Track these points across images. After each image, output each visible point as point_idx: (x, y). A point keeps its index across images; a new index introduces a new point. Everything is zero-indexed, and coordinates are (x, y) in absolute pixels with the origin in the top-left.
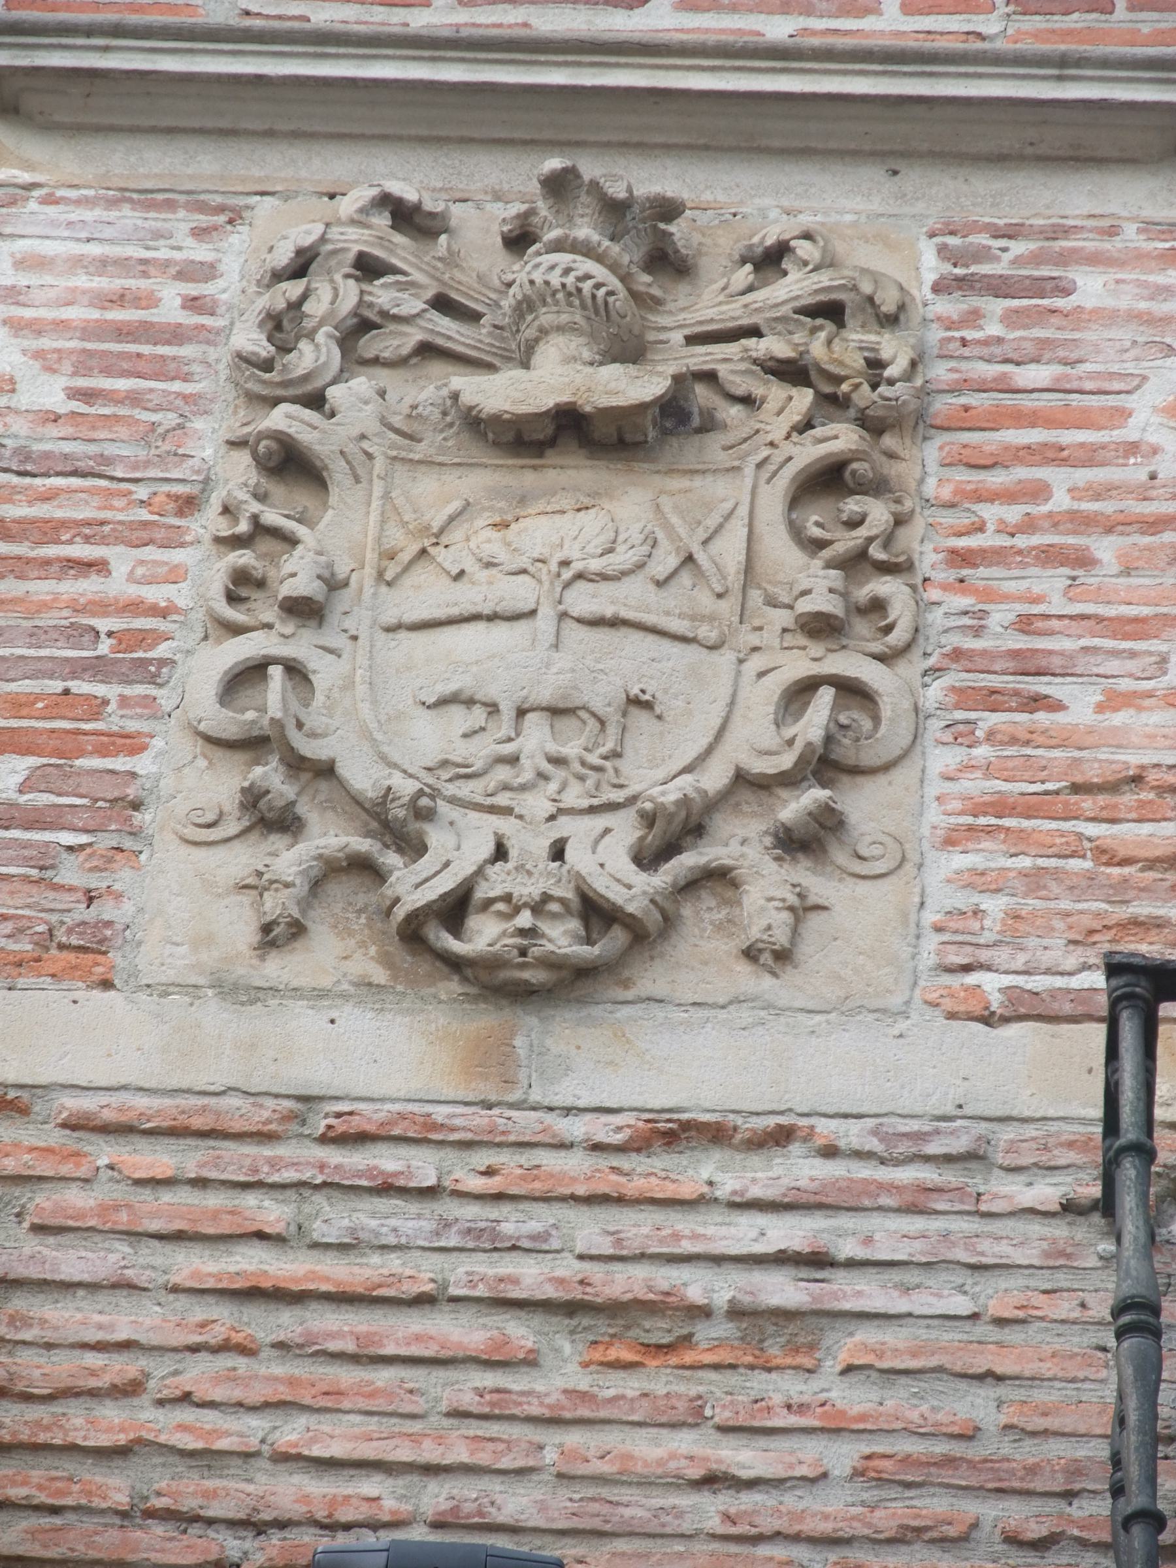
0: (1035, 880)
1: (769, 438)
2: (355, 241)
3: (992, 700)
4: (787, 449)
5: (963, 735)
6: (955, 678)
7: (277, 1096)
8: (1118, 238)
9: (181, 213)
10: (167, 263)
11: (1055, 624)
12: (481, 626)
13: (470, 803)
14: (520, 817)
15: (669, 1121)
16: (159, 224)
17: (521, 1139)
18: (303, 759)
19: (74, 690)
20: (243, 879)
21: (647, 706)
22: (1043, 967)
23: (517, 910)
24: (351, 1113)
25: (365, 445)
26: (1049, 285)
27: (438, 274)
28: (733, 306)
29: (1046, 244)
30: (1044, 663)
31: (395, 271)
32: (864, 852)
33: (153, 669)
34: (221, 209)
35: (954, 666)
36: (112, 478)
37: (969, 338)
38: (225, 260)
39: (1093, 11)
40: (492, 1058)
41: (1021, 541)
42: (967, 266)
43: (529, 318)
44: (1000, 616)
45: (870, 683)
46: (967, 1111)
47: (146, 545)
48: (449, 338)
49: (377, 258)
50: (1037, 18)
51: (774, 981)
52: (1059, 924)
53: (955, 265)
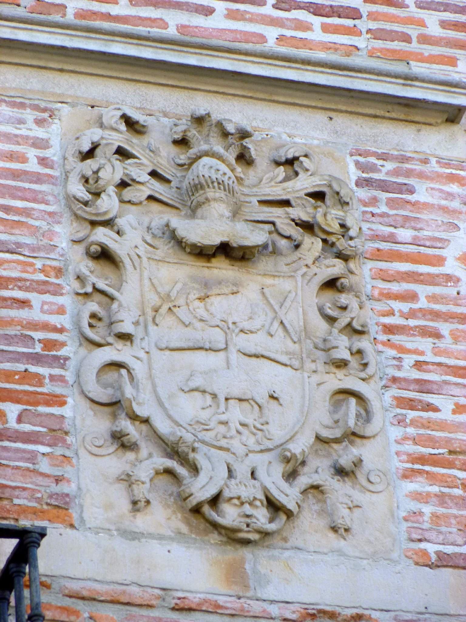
0: (442, 499)
1: (305, 262)
2: (116, 140)
3: (411, 404)
4: (314, 269)
5: (401, 422)
6: (395, 392)
7: (152, 587)
8: (428, 165)
9: (28, 110)
10: (27, 137)
11: (431, 367)
12: (203, 353)
13: (211, 444)
14: (234, 454)
15: (313, 609)
16: (20, 116)
17: (255, 615)
18: (137, 416)
19: (30, 370)
20: (120, 476)
21: (276, 399)
22: (450, 542)
23: (242, 504)
24: (184, 598)
25: (137, 251)
26: (404, 188)
27: (152, 160)
28: (278, 188)
29: (400, 165)
30: (429, 387)
31: (134, 157)
32: (372, 479)
33: (62, 361)
34: (44, 110)
35: (394, 386)
36: (24, 255)
37: (374, 212)
38: (52, 138)
39: (403, 41)
40: (236, 575)
41: (412, 323)
42: (368, 173)
43: (201, 192)
44: (409, 360)
45: (365, 394)
46: (429, 610)
47: (46, 293)
48: (161, 194)
49: (126, 150)
50: (380, 41)
51: (345, 542)
52: (453, 521)
53: (363, 172)
